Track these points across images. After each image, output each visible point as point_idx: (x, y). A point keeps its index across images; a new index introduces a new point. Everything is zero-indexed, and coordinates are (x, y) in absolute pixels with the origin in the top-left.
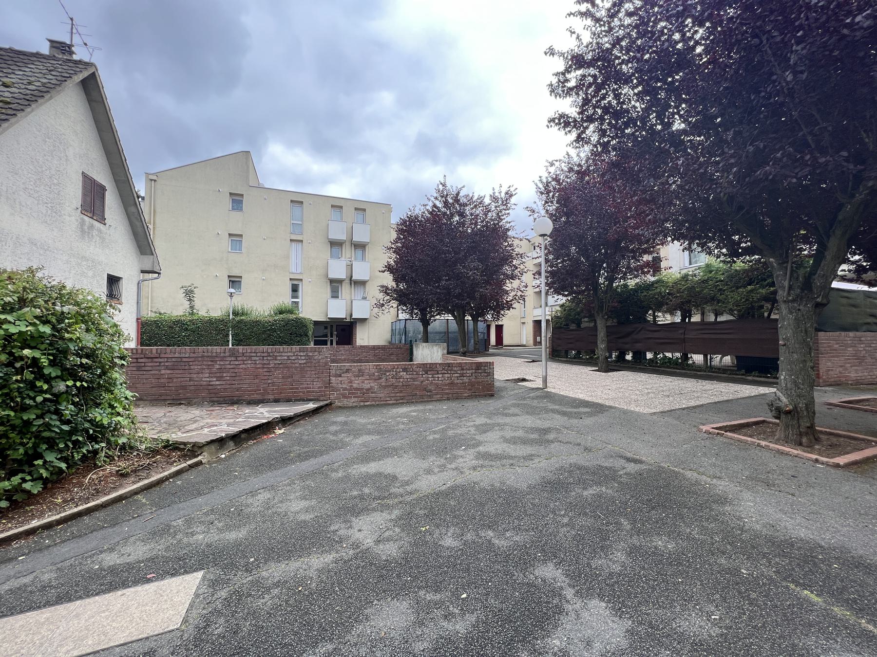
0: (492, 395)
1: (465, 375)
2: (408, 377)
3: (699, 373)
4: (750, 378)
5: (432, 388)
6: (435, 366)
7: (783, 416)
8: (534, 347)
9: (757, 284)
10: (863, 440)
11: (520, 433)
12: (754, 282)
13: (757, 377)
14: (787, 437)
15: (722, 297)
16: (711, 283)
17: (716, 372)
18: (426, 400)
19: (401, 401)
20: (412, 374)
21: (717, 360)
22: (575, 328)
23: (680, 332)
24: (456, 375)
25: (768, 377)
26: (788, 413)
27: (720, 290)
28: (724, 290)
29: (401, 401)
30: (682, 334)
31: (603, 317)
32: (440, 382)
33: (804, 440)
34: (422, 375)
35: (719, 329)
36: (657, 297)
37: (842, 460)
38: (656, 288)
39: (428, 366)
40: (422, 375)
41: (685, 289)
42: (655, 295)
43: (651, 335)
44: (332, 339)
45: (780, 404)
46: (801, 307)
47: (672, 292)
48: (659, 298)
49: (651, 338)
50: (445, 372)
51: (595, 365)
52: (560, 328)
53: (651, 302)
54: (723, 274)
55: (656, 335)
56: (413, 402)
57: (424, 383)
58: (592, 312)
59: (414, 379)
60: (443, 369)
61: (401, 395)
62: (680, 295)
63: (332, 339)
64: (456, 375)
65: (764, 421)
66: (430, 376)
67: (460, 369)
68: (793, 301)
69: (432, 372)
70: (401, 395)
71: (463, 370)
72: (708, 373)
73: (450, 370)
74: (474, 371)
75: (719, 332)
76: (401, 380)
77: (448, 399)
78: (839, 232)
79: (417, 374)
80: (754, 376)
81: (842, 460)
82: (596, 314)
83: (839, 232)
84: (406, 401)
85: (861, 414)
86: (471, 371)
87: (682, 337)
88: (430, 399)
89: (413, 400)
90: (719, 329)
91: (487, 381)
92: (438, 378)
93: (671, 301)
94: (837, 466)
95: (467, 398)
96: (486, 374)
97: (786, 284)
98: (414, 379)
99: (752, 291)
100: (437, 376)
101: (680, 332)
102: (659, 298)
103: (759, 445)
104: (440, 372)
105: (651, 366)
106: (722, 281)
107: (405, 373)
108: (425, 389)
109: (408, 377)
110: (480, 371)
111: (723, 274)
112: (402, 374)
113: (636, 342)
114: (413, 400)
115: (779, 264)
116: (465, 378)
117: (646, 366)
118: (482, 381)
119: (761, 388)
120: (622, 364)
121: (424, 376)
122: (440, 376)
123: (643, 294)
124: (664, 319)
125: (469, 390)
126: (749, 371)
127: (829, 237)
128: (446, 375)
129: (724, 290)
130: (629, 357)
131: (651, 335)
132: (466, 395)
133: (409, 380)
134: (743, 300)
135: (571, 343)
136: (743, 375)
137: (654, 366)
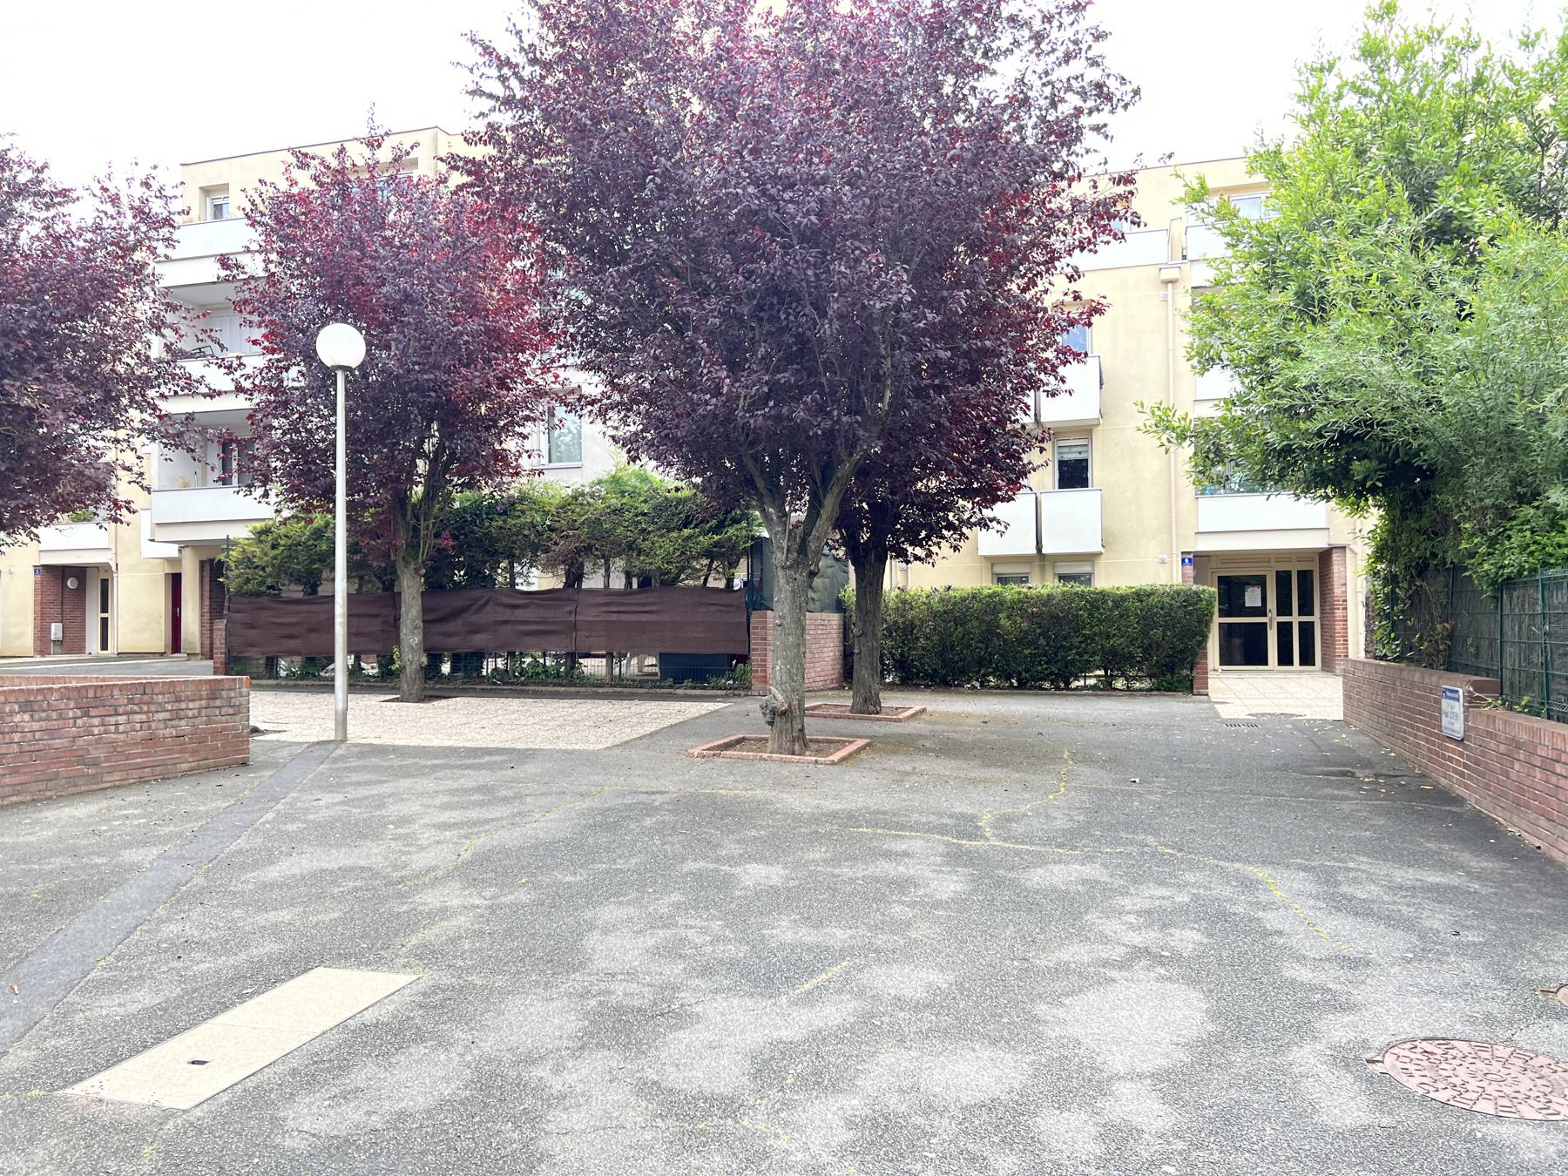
0: (244, 764)
1: (182, 713)
2: (36, 726)
3: (600, 690)
4: (680, 692)
5: (98, 753)
6: (108, 693)
7: (777, 719)
8: (39, 659)
9: (696, 526)
10: (838, 741)
11: (445, 799)
12: (691, 523)
13: (691, 688)
14: (780, 747)
15: (645, 545)
16: (627, 515)
17: (629, 686)
18: (83, 788)
19: (14, 799)
20: (48, 719)
21: (631, 666)
22: (301, 595)
23: (568, 609)
24: (162, 716)
25: (705, 688)
26: (784, 713)
27: (644, 530)
28: (649, 533)
29: (14, 799)
30: (570, 612)
31: (417, 571)
32: (122, 737)
33: (797, 747)
34: (75, 718)
35: (635, 604)
36: (526, 532)
37: (836, 757)
38: (523, 512)
39: (91, 694)
40: (75, 718)
41: (583, 523)
42: (523, 527)
43: (506, 615)
44: (105, 615)
45: (777, 704)
46: (797, 576)
47: (557, 525)
48: (532, 537)
49: (506, 622)
50: (135, 708)
51: (394, 689)
52: (258, 594)
53: (514, 542)
54: (645, 501)
55: (520, 614)
56: (50, 798)
57: (80, 742)
58: (393, 558)
59: (53, 734)
60: (131, 701)
61: (16, 779)
62: (574, 535)
63: (105, 615)
64: (162, 716)
65: (744, 739)
66: (96, 721)
67: (171, 697)
68: (790, 567)
69: (101, 711)
70: (16, 779)
71: (178, 700)
72: (617, 688)
73: (147, 703)
74: (204, 703)
75: (635, 608)
76: (16, 737)
77: (143, 781)
78: (836, 490)
79: (60, 718)
80: (687, 688)
81: (836, 757)
82: (400, 565)
83: (836, 490)
84: (29, 798)
85: (822, 721)
86: (197, 704)
87: (572, 619)
88: (95, 787)
89: (48, 794)
90: (635, 604)
91: (234, 728)
92: (117, 725)
93: (556, 544)
94: (833, 763)
95: (186, 774)
96: (231, 711)
97: (785, 544)
98: (53, 734)
99: (689, 538)
100: (112, 720)
101: (568, 609)
102: (532, 537)
103: (761, 759)
104: (121, 710)
105: (505, 684)
106: (645, 514)
107: (27, 717)
108: (81, 760)
109: (36, 726)
110: (218, 703)
111: (645, 501)
112: (17, 718)
113: (475, 632)
114: (48, 794)
115: (778, 517)
116: (183, 722)
117: (495, 683)
118: (224, 729)
119: (706, 704)
120: (436, 683)
121: (79, 722)
122: (122, 719)
123: (494, 524)
124: (538, 579)
125: (194, 752)
126: (678, 680)
127: (825, 492)
128: (138, 717)
129: (649, 533)
130: (446, 668)
131: (506, 615)
132: (185, 766)
133: (38, 735)
134: (678, 553)
135: (291, 637)
136: (670, 687)
137: (512, 684)
